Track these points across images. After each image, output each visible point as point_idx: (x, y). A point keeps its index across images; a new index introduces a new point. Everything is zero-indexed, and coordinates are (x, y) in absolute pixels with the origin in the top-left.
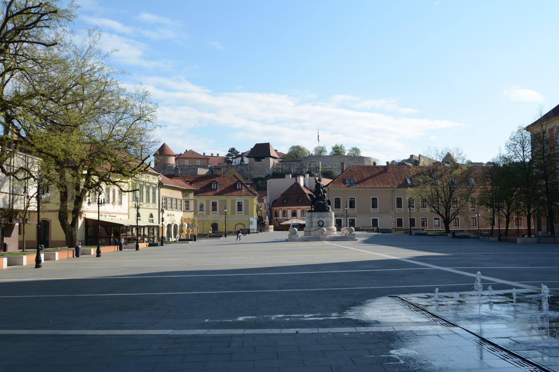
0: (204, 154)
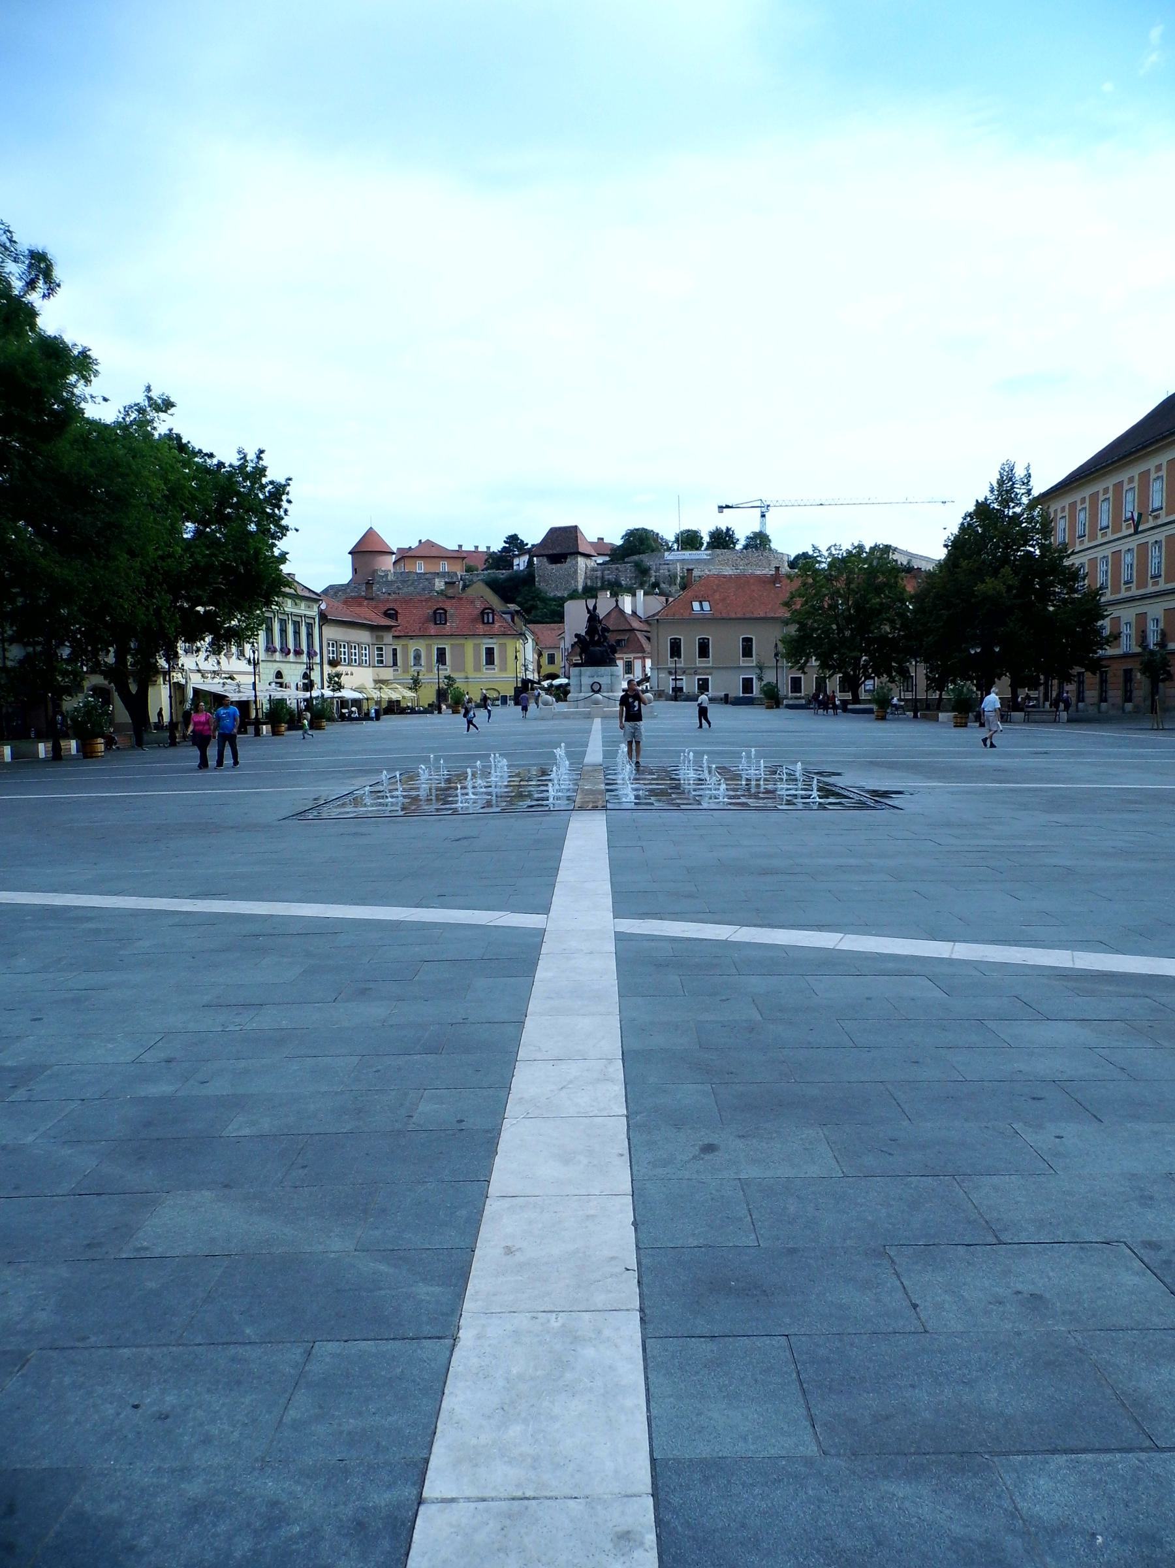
0: (488, 548)
